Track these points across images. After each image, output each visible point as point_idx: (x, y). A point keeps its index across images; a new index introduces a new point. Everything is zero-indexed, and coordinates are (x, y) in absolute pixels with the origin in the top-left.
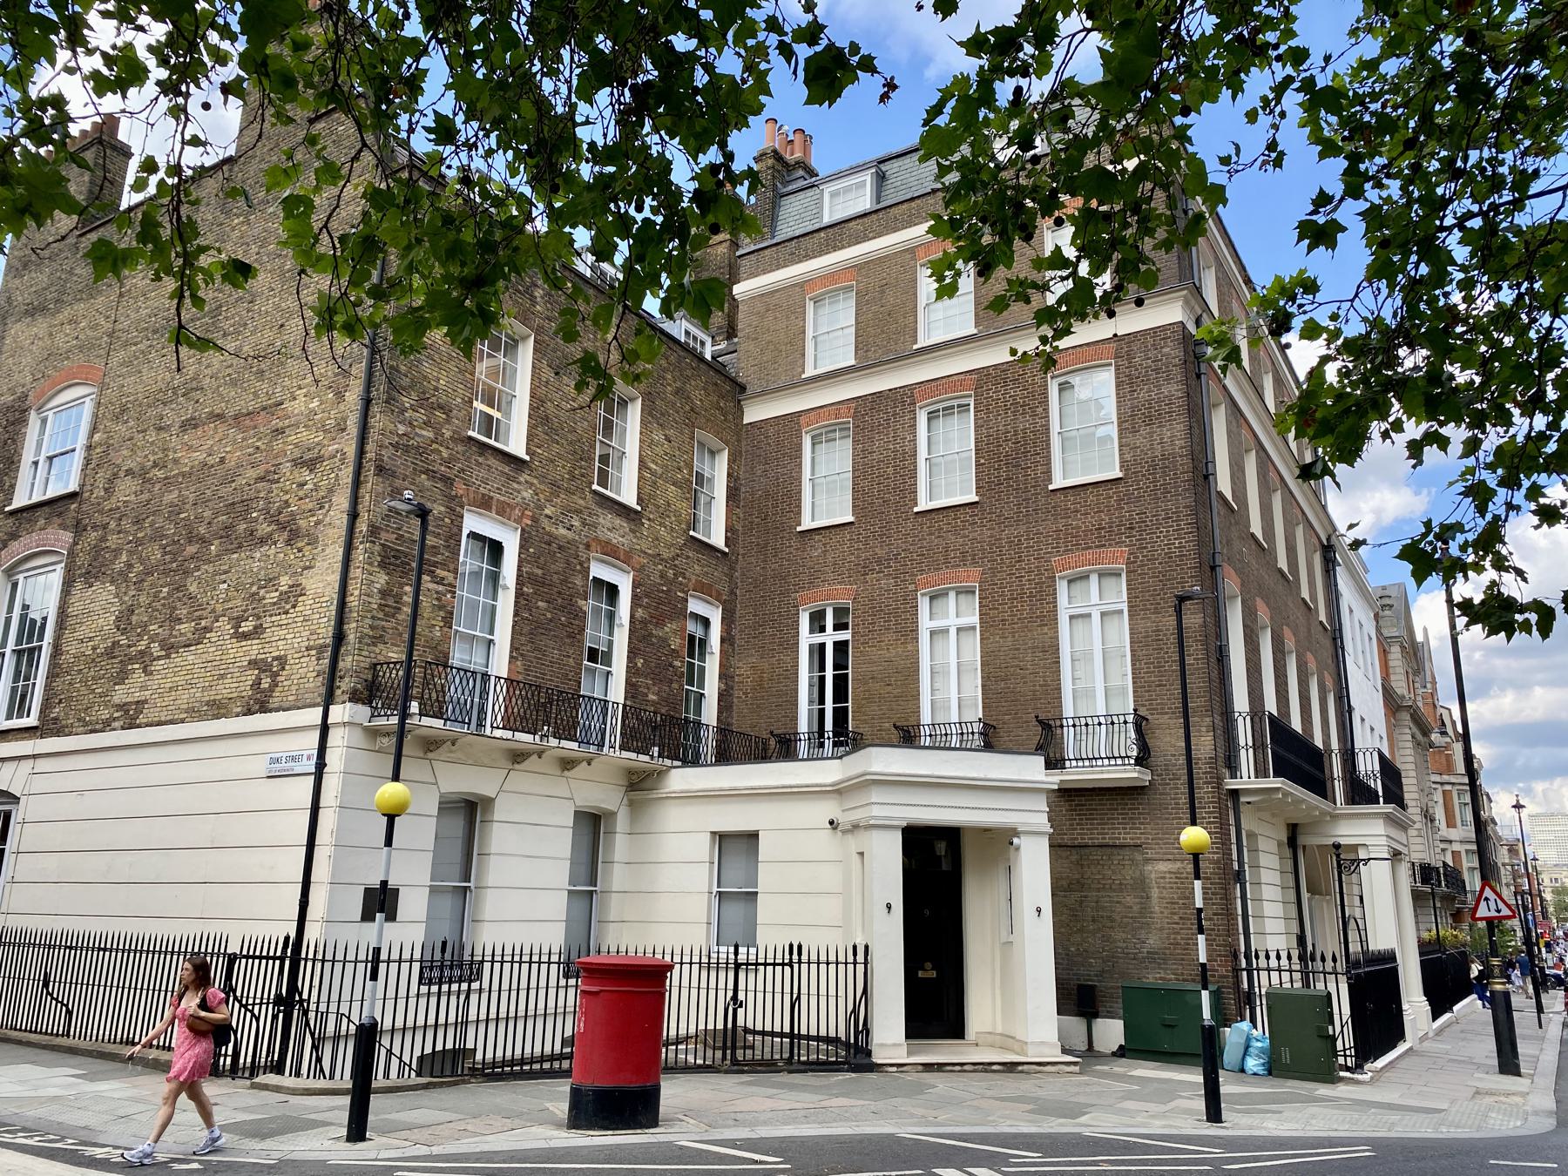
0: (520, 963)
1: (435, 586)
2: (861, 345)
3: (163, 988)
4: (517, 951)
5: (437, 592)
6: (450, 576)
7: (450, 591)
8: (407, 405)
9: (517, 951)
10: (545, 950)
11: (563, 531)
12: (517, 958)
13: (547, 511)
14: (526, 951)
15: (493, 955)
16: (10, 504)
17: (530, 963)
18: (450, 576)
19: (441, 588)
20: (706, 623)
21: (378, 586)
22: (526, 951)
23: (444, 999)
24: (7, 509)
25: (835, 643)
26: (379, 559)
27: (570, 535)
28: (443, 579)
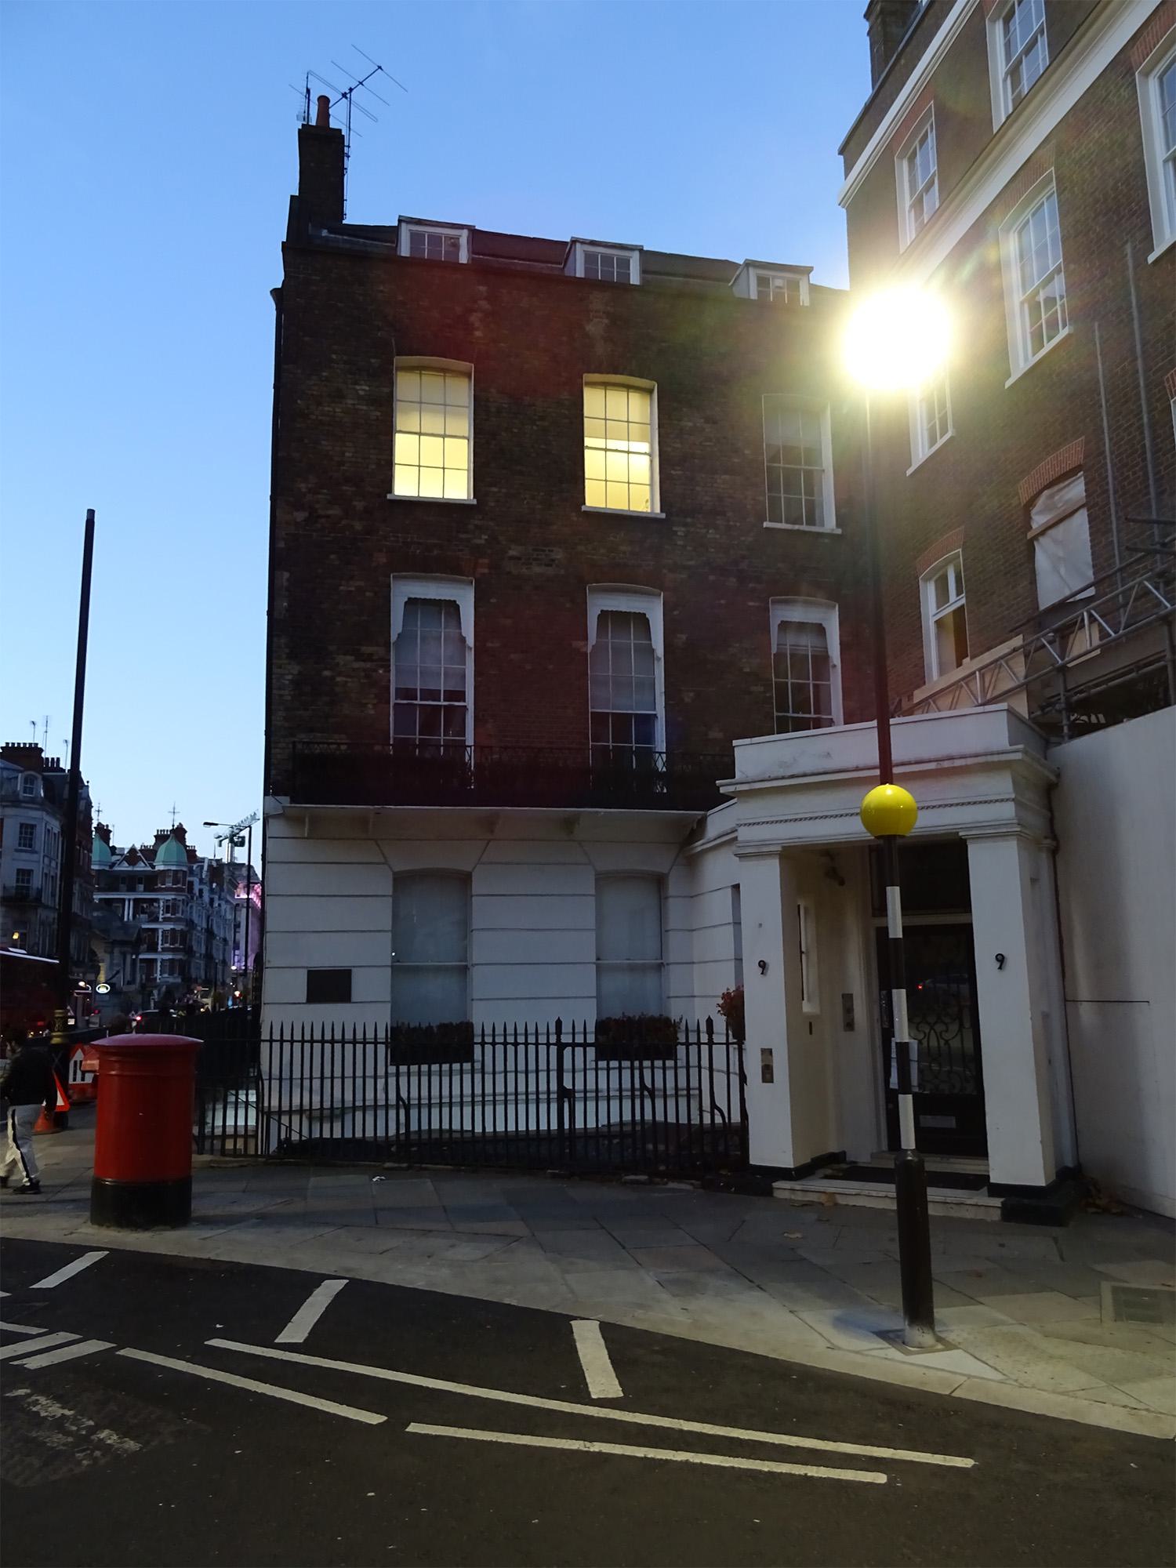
0: (494, 1044)
1: (361, 665)
2: (812, 284)
3: (359, 1073)
4: (511, 1031)
5: (365, 670)
6: (379, 651)
7: (382, 667)
8: (304, 490)
9: (511, 1031)
10: (531, 1029)
11: (537, 569)
12: (510, 1039)
13: (512, 553)
14: (499, 1030)
15: (483, 1035)
16: (1152, 249)
17: (505, 1044)
18: (379, 651)
19: (369, 665)
20: (820, 630)
21: (290, 677)
22: (499, 1030)
23: (424, 1080)
24: (1151, 259)
25: (419, 735)
26: (287, 651)
27: (550, 571)
28: (372, 654)
